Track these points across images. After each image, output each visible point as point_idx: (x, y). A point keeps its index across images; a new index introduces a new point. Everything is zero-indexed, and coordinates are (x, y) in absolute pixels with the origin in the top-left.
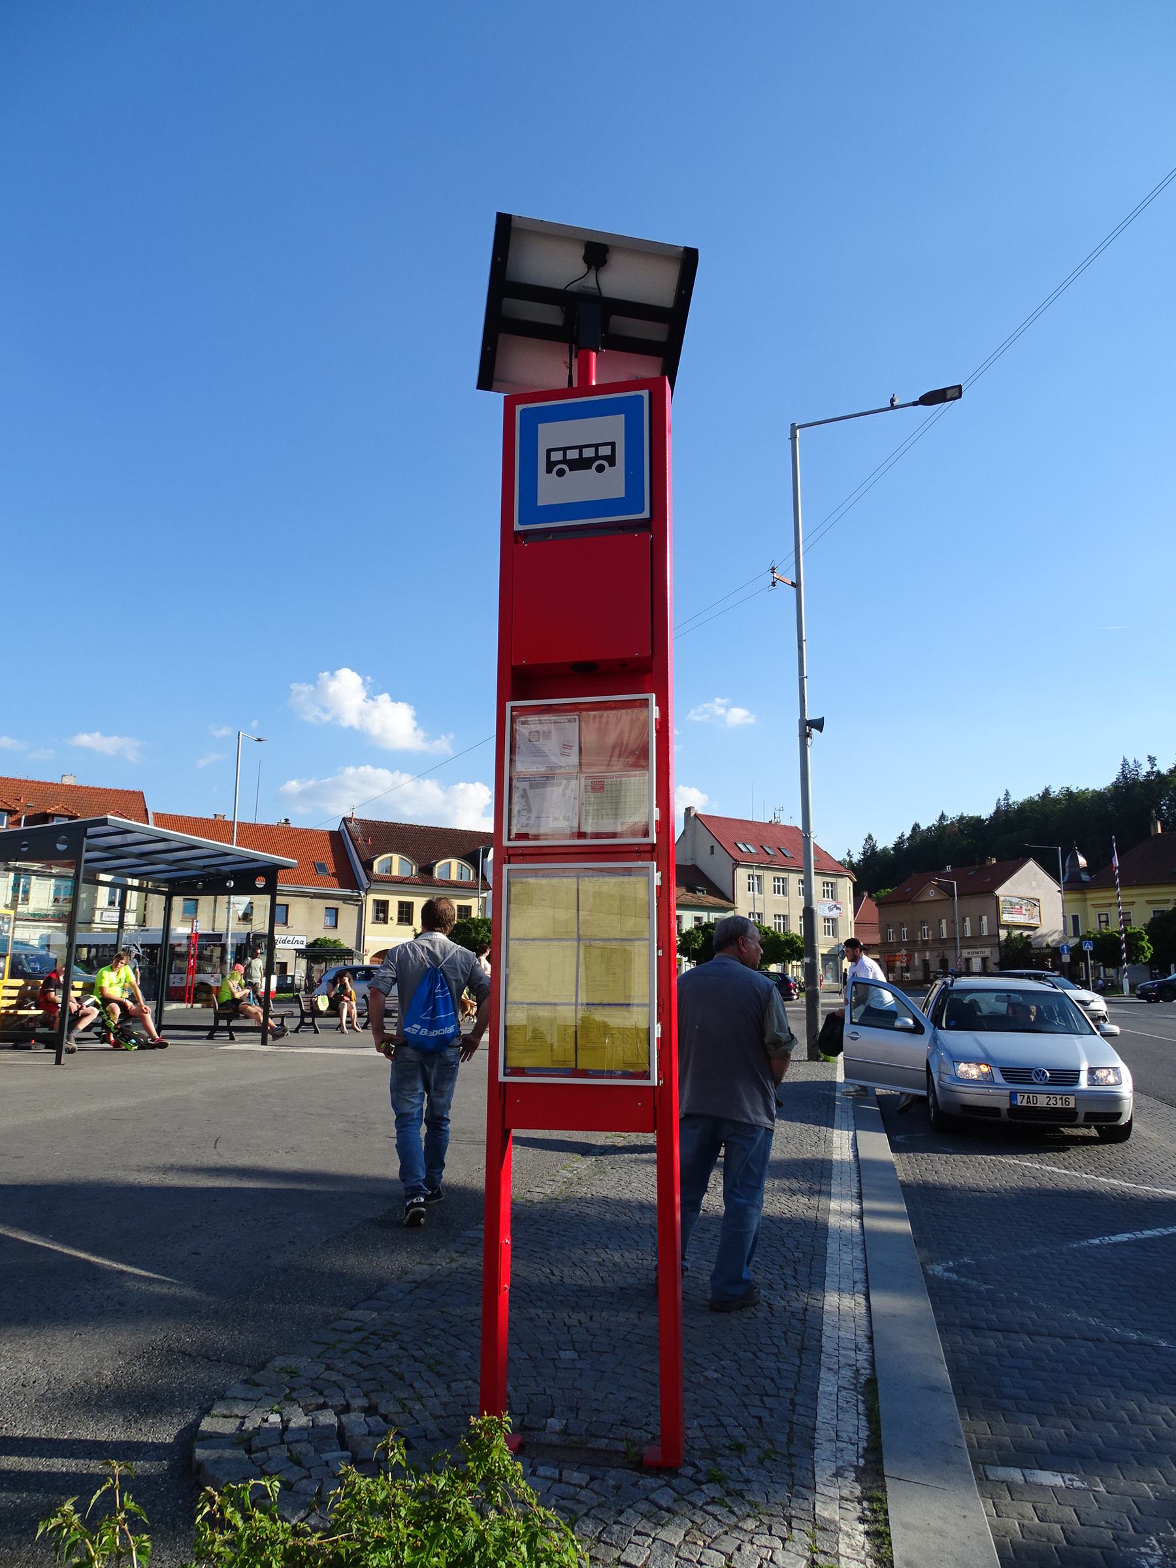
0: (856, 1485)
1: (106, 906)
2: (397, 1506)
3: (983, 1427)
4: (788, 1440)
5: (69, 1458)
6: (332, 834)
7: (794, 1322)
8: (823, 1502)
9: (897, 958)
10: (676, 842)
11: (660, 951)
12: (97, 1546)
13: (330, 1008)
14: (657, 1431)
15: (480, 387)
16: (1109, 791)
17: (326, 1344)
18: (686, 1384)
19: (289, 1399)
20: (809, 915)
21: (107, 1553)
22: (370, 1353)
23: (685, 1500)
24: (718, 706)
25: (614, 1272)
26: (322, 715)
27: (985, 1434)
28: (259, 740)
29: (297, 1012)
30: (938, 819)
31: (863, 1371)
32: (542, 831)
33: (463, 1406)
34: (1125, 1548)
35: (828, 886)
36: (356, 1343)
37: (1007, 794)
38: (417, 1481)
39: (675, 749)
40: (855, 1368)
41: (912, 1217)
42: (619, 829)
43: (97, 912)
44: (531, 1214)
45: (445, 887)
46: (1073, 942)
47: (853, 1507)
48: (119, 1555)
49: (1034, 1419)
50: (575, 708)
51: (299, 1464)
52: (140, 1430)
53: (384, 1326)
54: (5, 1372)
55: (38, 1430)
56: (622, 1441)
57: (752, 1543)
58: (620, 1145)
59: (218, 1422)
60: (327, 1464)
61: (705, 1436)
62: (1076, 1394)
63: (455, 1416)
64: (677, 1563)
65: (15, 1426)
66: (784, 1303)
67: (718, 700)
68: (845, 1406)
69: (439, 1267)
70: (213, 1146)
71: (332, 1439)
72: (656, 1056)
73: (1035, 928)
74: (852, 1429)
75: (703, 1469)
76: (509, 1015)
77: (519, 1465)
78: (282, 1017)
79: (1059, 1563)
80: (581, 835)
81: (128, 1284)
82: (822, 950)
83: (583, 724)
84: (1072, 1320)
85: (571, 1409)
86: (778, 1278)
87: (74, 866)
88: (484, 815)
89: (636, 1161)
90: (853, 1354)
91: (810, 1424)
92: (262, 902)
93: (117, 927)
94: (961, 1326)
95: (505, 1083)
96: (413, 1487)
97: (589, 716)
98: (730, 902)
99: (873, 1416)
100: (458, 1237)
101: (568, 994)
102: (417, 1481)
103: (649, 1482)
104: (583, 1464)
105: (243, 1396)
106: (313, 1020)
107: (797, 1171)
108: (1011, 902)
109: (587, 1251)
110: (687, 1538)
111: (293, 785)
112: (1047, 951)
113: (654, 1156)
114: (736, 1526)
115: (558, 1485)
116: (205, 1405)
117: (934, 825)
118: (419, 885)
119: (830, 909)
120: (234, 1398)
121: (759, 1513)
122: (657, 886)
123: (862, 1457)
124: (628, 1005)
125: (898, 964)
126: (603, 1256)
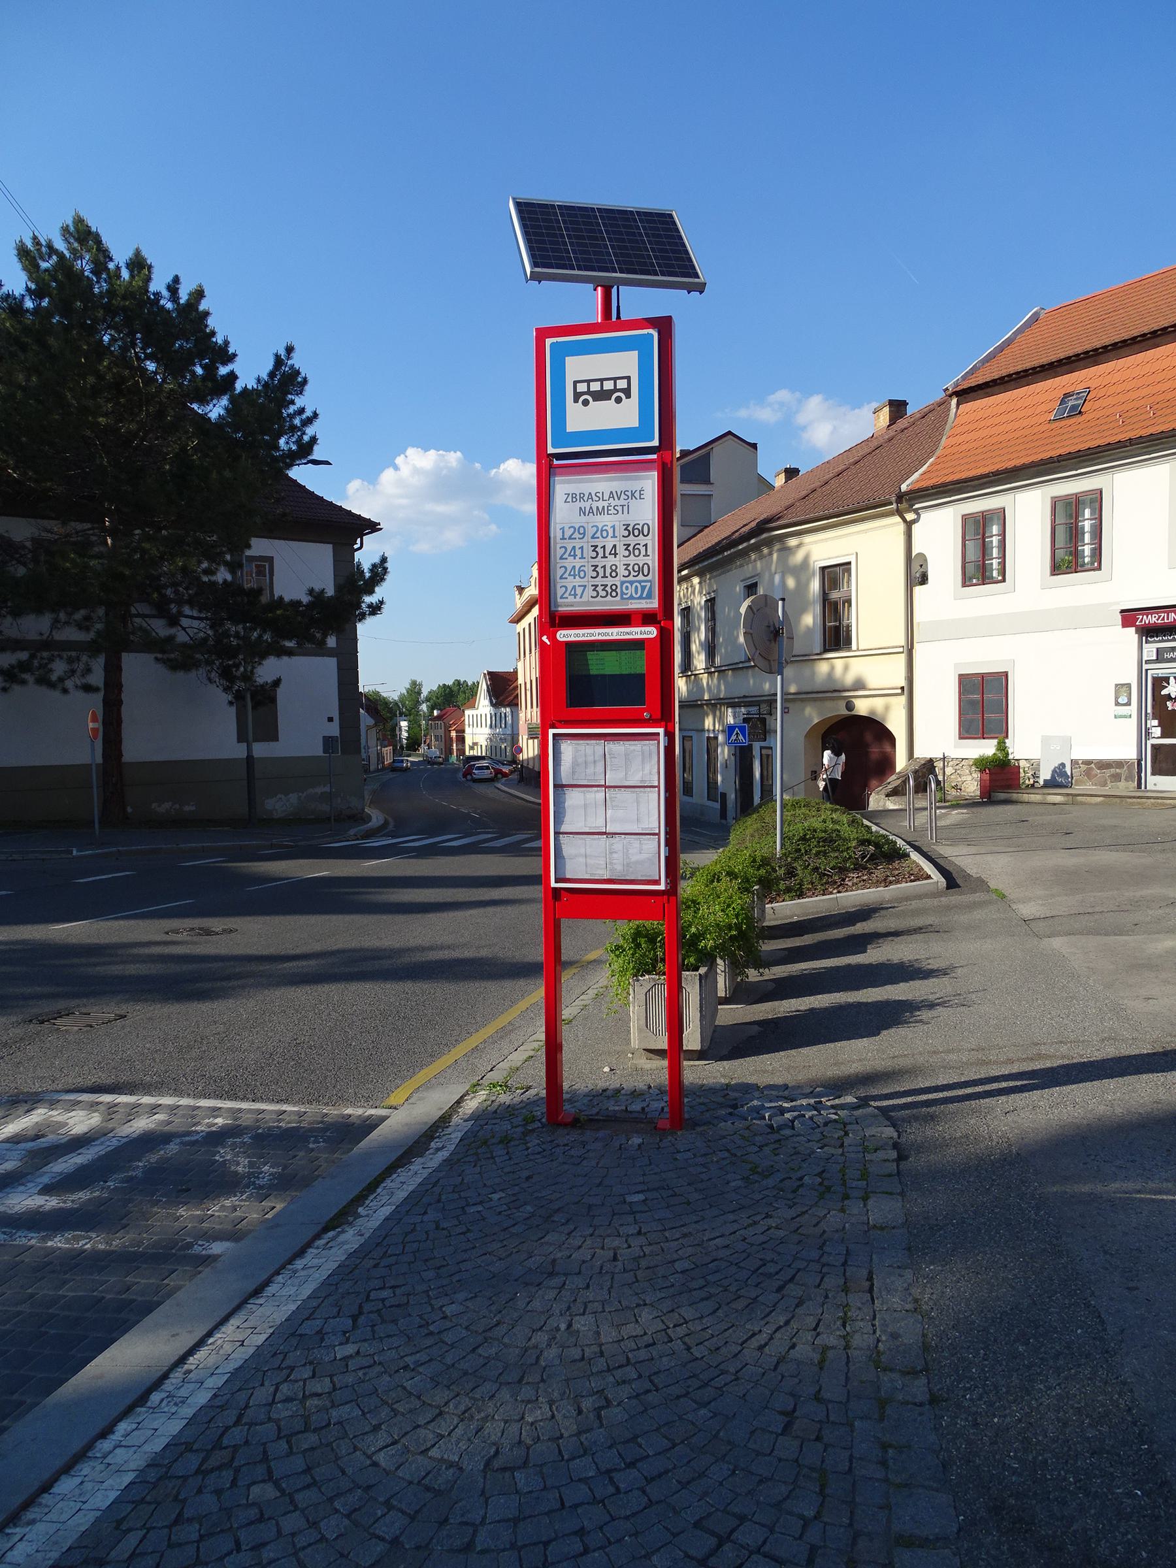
55: (952, 1107)
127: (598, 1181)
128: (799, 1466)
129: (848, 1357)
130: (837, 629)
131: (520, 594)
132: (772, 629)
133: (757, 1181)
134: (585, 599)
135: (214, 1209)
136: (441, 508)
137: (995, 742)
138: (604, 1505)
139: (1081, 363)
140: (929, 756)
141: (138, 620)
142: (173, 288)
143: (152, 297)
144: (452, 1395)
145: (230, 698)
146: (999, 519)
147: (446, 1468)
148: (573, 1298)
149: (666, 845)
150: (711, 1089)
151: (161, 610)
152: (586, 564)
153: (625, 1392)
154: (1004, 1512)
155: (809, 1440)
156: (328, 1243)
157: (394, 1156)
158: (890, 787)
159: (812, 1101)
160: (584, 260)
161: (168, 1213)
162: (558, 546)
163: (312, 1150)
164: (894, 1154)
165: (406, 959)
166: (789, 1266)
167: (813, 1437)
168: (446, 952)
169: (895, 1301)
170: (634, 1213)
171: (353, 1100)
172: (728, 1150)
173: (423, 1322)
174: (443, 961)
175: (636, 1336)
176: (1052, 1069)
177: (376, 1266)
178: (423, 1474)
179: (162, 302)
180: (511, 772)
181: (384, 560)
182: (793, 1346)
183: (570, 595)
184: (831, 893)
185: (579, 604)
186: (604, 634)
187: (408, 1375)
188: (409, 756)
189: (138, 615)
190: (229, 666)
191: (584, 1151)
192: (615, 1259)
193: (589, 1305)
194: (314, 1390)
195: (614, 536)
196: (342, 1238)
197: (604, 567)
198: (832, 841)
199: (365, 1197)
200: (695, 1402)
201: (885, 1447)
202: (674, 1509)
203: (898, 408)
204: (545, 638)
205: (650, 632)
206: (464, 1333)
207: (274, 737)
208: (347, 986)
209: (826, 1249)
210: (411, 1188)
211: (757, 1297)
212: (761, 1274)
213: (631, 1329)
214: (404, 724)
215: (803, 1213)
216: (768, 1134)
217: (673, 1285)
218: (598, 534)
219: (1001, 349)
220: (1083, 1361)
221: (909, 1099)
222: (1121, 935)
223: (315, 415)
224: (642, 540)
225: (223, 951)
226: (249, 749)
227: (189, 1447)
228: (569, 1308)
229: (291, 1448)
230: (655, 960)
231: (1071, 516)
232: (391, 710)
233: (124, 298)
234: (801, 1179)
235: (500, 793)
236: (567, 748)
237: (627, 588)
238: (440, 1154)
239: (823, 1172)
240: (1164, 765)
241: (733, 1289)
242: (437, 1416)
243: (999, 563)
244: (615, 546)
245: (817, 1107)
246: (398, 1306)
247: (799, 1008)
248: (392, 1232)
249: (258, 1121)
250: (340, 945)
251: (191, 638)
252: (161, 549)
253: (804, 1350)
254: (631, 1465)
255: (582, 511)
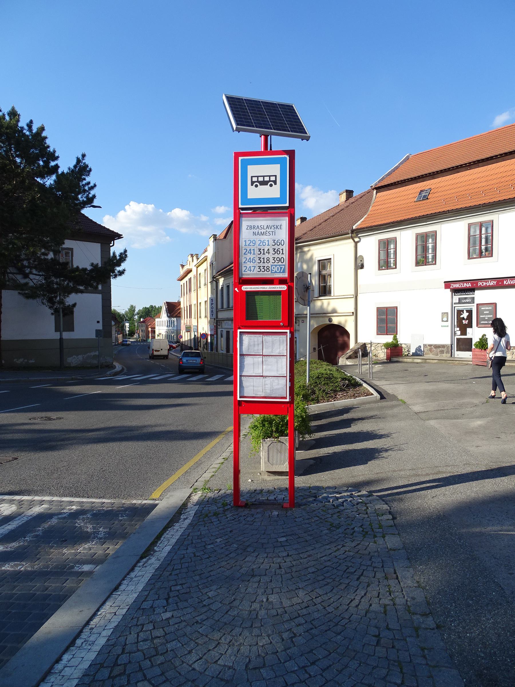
11: (487, 318)
127: (263, 532)
128: (388, 660)
129: (396, 609)
130: (325, 287)
131: (182, 268)
132: (305, 286)
133: (334, 530)
134: (255, 272)
135: (81, 549)
136: (145, 229)
137: (392, 336)
138: (306, 683)
139: (428, 178)
140: (364, 342)
141: (10, 275)
142: (30, 125)
143: (20, 129)
144: (222, 634)
145: (52, 311)
146: (394, 242)
147: (228, 669)
148: (266, 587)
149: (290, 381)
150: (303, 489)
151: (21, 271)
152: (255, 257)
153: (301, 629)
154: (483, 677)
155: (389, 648)
156: (144, 564)
157: (166, 523)
158: (348, 355)
159: (349, 494)
160: (258, 123)
161: (59, 552)
162: (243, 249)
163: (121, 520)
164: (390, 517)
165: (145, 431)
166: (359, 568)
167: (391, 647)
168: (163, 428)
169: (409, 582)
170: (283, 546)
171: (135, 496)
172: (318, 517)
173: (200, 601)
174: (162, 432)
175: (299, 603)
176: (446, 478)
177: (171, 574)
178: (218, 673)
179: (24, 131)
180: (177, 347)
181: (125, 251)
182: (371, 605)
183: (248, 270)
184: (331, 401)
185: (253, 274)
186: (263, 288)
187: (199, 626)
188: (130, 339)
189: (11, 273)
190: (53, 297)
191: (253, 518)
192: (280, 568)
193: (274, 590)
194: (156, 635)
195: (269, 245)
196: (150, 562)
197: (264, 258)
198: (330, 378)
199: (157, 542)
200: (334, 632)
201: (423, 649)
202: (338, 683)
203: (349, 193)
204: (236, 289)
205: (284, 288)
206: (220, 605)
207: (72, 330)
208: (121, 443)
209: (373, 560)
210: (177, 537)
211: (349, 583)
212: (348, 572)
213: (295, 600)
214: (127, 325)
215: (358, 544)
216: (333, 509)
217: (310, 579)
218: (261, 244)
219: (394, 170)
220: (499, 607)
221: (389, 492)
222: (457, 419)
223: (95, 185)
224: (281, 247)
225: (59, 428)
226: (61, 335)
227: (102, 665)
228: (265, 591)
229: (152, 663)
230: (272, 431)
231: (423, 242)
232: (121, 318)
233: (7, 128)
234: (353, 529)
235: (173, 356)
236: (246, 338)
237: (274, 268)
238: (186, 521)
239: (362, 525)
240: (461, 347)
241: (337, 579)
242: (217, 645)
243: (394, 261)
244: (268, 249)
245: (351, 496)
246: (186, 593)
247: (329, 452)
248: (174, 558)
249: (92, 507)
250: (113, 425)
251: (35, 284)
252: (23, 243)
253: (375, 607)
254: (313, 663)
255: (254, 233)
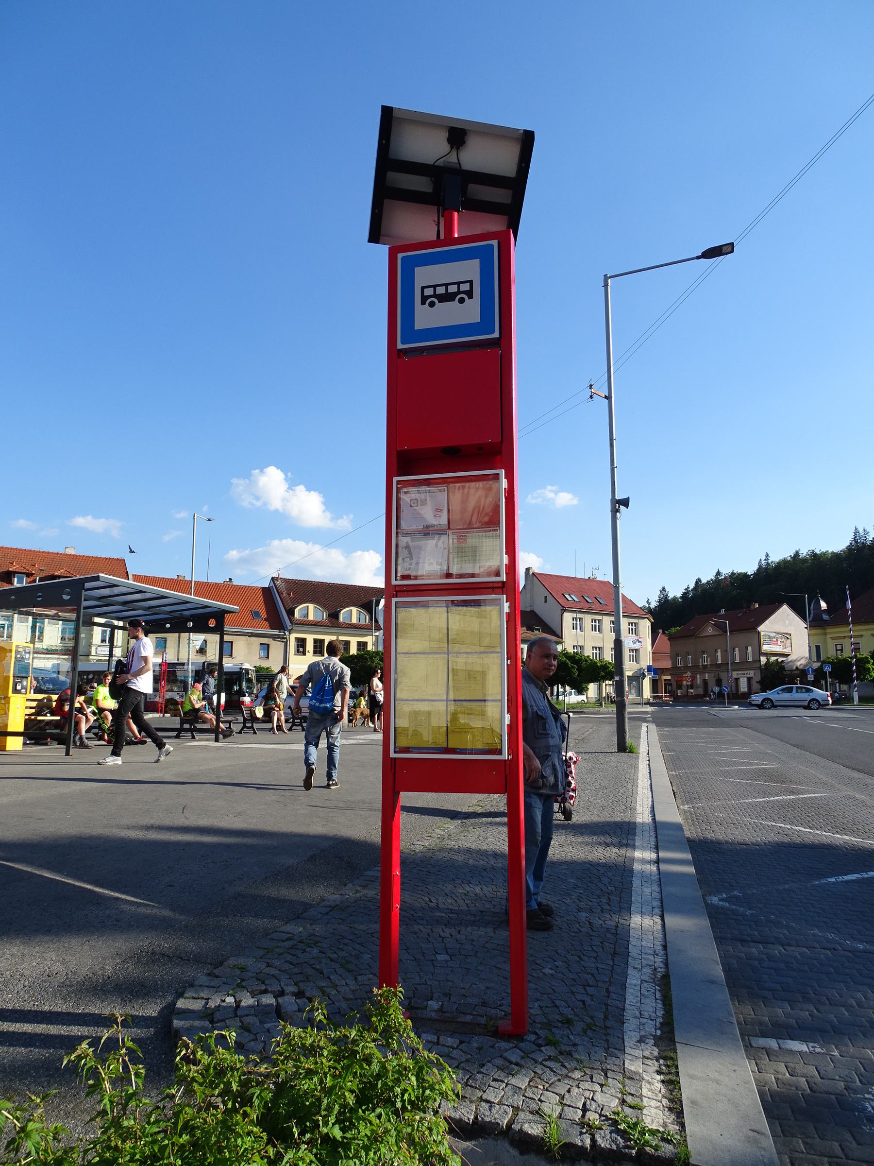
0: (655, 1048)
1: (99, 643)
2: (322, 1048)
3: (748, 1010)
4: (604, 1016)
5: (83, 1026)
6: (264, 589)
7: (608, 935)
8: (630, 1060)
9: (684, 679)
10: (520, 590)
11: (509, 661)
12: (106, 1071)
13: (265, 715)
14: (509, 1010)
15: (370, 241)
16: (844, 552)
17: (266, 949)
18: (529, 978)
19: (241, 987)
20: (618, 645)
21: (114, 1076)
22: (299, 956)
23: (528, 1057)
24: (549, 492)
25: (476, 900)
26: (255, 502)
27: (750, 1015)
28: (209, 520)
29: (241, 719)
30: (715, 575)
31: (659, 970)
32: (420, 573)
33: (366, 992)
34: (854, 1094)
35: (632, 625)
36: (288, 949)
37: (767, 555)
38: (335, 1032)
39: (519, 512)
40: (653, 967)
41: (696, 863)
42: (477, 571)
43: (93, 647)
44: (414, 860)
45: (349, 628)
46: (816, 665)
47: (652, 1064)
48: (122, 1079)
49: (786, 1005)
50: (444, 481)
51: (249, 1031)
52: (133, 1007)
53: (308, 937)
54: (35, 967)
55: (60, 1007)
56: (483, 1016)
57: (579, 1088)
58: (479, 812)
59: (189, 1003)
60: (268, 1031)
61: (544, 1014)
62: (817, 987)
63: (361, 999)
64: (523, 1100)
65: (44, 1004)
66: (601, 922)
67: (549, 487)
68: (646, 993)
69: (348, 896)
70: (181, 811)
71: (271, 1013)
72: (507, 738)
73: (787, 655)
74: (651, 1010)
75: (542, 1036)
76: (397, 720)
77: (409, 1022)
78: (230, 722)
79: (804, 1105)
80: (448, 575)
81: (122, 907)
82: (628, 673)
83: (450, 493)
84: (814, 935)
85: (445, 995)
86: (596, 904)
87: (76, 612)
88: (375, 575)
89: (491, 823)
90: (652, 958)
91: (621, 1006)
92: (213, 639)
93: (107, 658)
94: (732, 939)
95: (395, 758)
96: (333, 1036)
97: (455, 486)
98: (559, 638)
99: (667, 1001)
100: (361, 876)
101: (441, 692)
102: (335, 1032)
103: (503, 1045)
104: (454, 1032)
105: (207, 984)
106: (253, 725)
107: (610, 830)
108: (769, 636)
109: (456, 885)
110: (531, 1083)
111: (234, 554)
112: (797, 672)
113: (506, 819)
114: (567, 1076)
115: (436, 1047)
116: (180, 991)
117: (712, 580)
118: (328, 626)
119: (634, 643)
120: (201, 986)
121: (584, 1067)
122: (506, 613)
123: (659, 1029)
124: (485, 701)
125: (685, 683)
126: (468, 889)
